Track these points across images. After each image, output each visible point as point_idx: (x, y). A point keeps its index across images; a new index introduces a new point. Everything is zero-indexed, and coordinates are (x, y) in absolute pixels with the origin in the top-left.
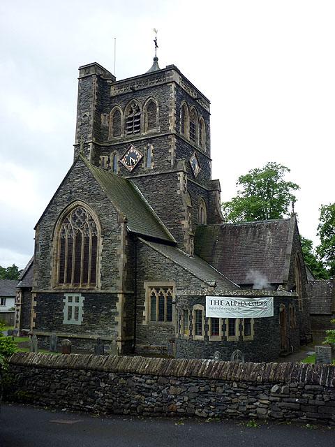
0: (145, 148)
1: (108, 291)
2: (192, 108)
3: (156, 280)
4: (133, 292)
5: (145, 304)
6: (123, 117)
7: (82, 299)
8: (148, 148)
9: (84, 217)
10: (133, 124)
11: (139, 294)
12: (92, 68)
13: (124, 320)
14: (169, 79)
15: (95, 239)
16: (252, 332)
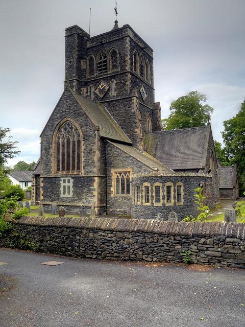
0: (111, 82)
2: (141, 54)
4: (104, 176)
5: (113, 183)
7: (72, 181)
8: (112, 82)
9: (72, 128)
10: (103, 67)
12: (74, 29)
14: (125, 34)
15: (79, 142)
16: (183, 200)
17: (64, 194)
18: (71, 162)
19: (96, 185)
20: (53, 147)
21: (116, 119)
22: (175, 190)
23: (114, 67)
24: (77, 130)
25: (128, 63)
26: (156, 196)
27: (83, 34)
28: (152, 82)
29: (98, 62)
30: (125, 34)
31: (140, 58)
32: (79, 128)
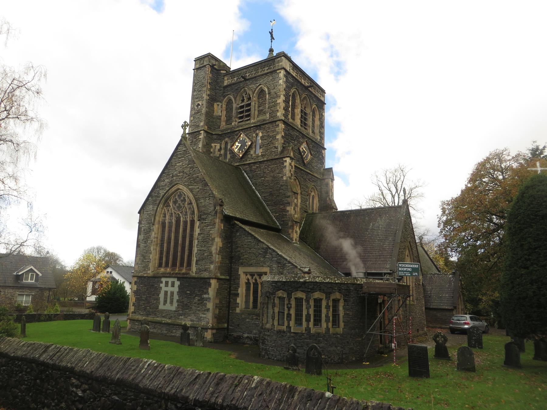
0: (254, 135)
1: (202, 276)
2: (303, 96)
3: (251, 265)
4: (228, 277)
5: (240, 291)
6: (234, 106)
7: (177, 283)
8: (257, 135)
9: (184, 200)
10: (245, 112)
11: (234, 280)
12: (206, 59)
13: (216, 306)
14: (278, 66)
15: (193, 222)
16: (342, 324)
17: (164, 304)
18: (179, 254)
19: (212, 292)
20: (153, 233)
21: (259, 191)
22: (328, 307)
23: (260, 112)
24: (191, 203)
25: (280, 108)
26: (296, 315)
27: (219, 66)
28: (322, 138)
29: (238, 106)
30: (278, 66)
31: (301, 101)
32: (193, 201)
